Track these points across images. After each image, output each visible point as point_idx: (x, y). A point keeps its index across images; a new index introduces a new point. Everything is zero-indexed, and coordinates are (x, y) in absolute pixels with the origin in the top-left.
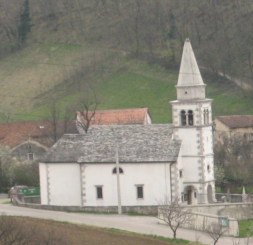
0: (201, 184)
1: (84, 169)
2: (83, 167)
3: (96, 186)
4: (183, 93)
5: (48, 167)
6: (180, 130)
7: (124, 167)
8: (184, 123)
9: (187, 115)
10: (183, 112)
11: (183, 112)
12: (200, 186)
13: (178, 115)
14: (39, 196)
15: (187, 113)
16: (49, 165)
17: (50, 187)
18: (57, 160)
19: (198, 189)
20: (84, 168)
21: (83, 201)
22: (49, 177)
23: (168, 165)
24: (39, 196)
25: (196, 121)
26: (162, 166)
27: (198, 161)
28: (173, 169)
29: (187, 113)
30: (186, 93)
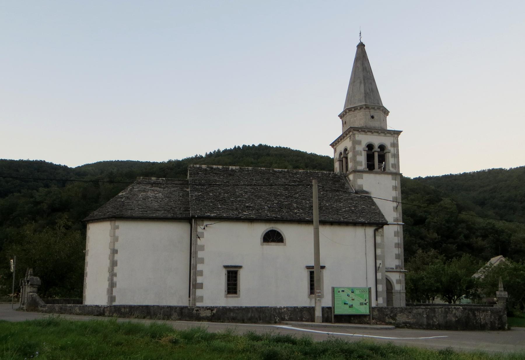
0: (401, 274)
1: (203, 231)
2: (203, 227)
3: (226, 267)
4: (369, 117)
5: (117, 228)
6: (365, 176)
7: (284, 229)
8: (371, 167)
9: (376, 151)
10: (370, 147)
11: (370, 147)
12: (398, 278)
13: (362, 150)
14: (316, 216)
15: (376, 148)
16: (118, 223)
17: (116, 269)
18: (136, 214)
19: (395, 282)
20: (204, 228)
21: (112, 298)
22: (116, 248)
23: (370, 231)
24: (316, 216)
25: (392, 164)
26: (359, 232)
27: (395, 232)
28: (378, 239)
29: (376, 148)
30: (373, 117)
